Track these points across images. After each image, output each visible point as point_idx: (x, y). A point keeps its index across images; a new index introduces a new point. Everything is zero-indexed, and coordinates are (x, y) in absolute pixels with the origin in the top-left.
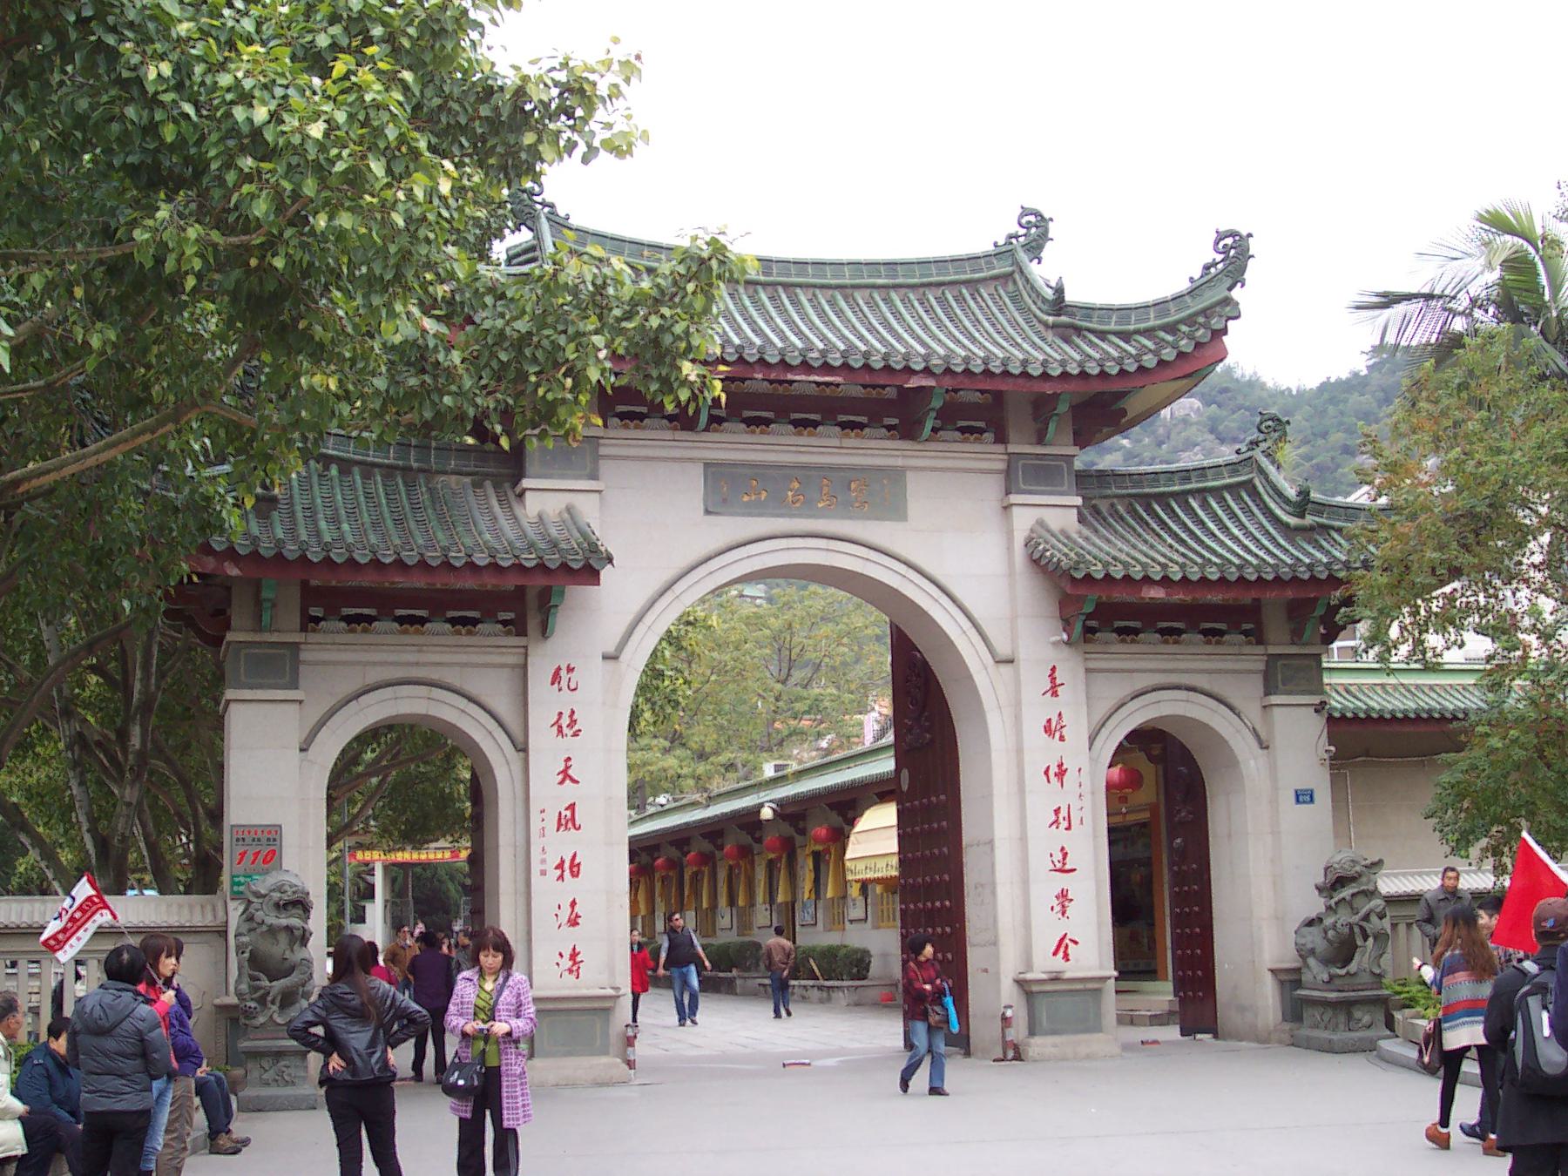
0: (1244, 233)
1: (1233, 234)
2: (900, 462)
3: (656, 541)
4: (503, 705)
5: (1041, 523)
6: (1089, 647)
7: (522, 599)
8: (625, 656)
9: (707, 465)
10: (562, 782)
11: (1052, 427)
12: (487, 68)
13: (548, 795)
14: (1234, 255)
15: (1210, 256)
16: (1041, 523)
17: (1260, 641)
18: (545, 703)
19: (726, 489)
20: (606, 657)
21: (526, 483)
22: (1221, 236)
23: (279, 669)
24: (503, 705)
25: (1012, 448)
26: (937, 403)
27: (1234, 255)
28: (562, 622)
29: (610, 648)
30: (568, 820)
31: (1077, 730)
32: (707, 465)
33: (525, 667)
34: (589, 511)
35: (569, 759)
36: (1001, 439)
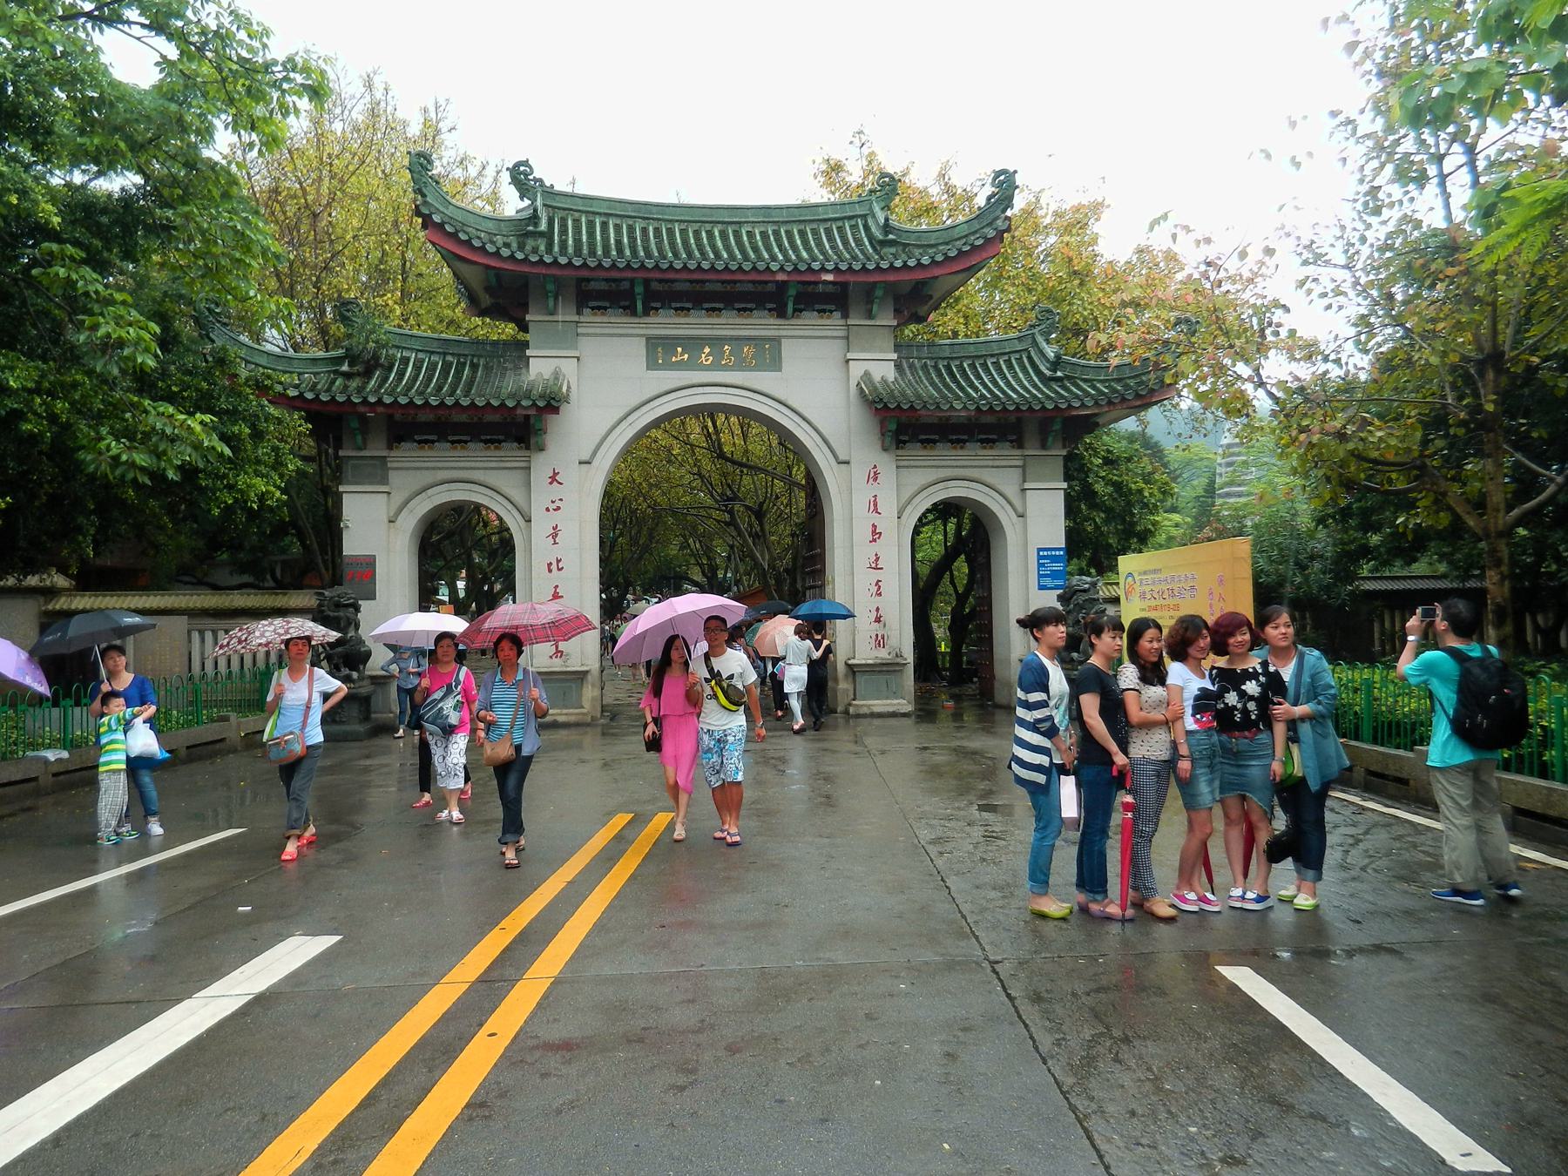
2: (776, 333)
3: (608, 389)
5: (867, 374)
6: (900, 452)
7: (520, 427)
8: (595, 463)
9: (649, 339)
11: (875, 308)
12: (916, 197)
16: (867, 374)
17: (1021, 446)
19: (659, 351)
21: (528, 353)
23: (377, 473)
24: (517, 496)
26: (792, 292)
28: (551, 440)
30: (876, 534)
31: (889, 506)
32: (649, 339)
34: (568, 368)
36: (845, 316)
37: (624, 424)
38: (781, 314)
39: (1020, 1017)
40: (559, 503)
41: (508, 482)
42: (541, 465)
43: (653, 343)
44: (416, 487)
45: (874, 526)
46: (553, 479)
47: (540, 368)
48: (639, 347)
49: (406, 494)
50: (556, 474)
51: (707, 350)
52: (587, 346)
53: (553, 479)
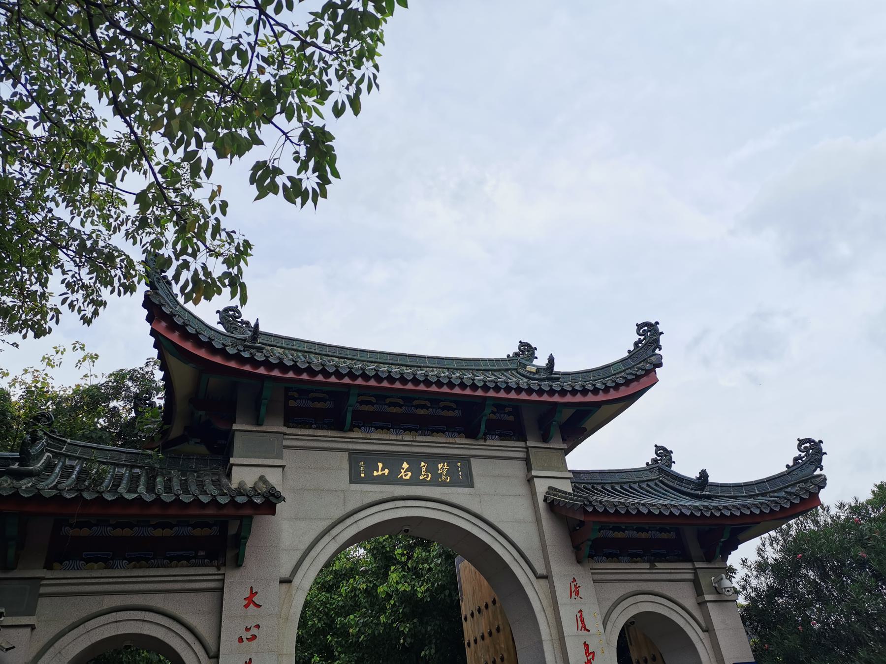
1: (809, 440)
8: (296, 581)
9: (352, 453)
10: (246, 606)
14: (650, 335)
15: (637, 338)
18: (234, 597)
19: (359, 467)
20: (282, 581)
22: (801, 442)
24: (203, 626)
25: (529, 444)
27: (650, 335)
29: (285, 572)
31: (594, 622)
32: (352, 453)
33: (221, 590)
37: (326, 539)
38: (472, 434)
39: (143, 621)
40: (254, 631)
41: (194, 611)
42: (236, 586)
43: (355, 457)
44: (615, 597)
45: (586, 645)
46: (250, 601)
47: (244, 476)
48: (342, 461)
49: (54, 630)
50: (253, 594)
51: (405, 465)
52: (289, 458)
53: (250, 601)
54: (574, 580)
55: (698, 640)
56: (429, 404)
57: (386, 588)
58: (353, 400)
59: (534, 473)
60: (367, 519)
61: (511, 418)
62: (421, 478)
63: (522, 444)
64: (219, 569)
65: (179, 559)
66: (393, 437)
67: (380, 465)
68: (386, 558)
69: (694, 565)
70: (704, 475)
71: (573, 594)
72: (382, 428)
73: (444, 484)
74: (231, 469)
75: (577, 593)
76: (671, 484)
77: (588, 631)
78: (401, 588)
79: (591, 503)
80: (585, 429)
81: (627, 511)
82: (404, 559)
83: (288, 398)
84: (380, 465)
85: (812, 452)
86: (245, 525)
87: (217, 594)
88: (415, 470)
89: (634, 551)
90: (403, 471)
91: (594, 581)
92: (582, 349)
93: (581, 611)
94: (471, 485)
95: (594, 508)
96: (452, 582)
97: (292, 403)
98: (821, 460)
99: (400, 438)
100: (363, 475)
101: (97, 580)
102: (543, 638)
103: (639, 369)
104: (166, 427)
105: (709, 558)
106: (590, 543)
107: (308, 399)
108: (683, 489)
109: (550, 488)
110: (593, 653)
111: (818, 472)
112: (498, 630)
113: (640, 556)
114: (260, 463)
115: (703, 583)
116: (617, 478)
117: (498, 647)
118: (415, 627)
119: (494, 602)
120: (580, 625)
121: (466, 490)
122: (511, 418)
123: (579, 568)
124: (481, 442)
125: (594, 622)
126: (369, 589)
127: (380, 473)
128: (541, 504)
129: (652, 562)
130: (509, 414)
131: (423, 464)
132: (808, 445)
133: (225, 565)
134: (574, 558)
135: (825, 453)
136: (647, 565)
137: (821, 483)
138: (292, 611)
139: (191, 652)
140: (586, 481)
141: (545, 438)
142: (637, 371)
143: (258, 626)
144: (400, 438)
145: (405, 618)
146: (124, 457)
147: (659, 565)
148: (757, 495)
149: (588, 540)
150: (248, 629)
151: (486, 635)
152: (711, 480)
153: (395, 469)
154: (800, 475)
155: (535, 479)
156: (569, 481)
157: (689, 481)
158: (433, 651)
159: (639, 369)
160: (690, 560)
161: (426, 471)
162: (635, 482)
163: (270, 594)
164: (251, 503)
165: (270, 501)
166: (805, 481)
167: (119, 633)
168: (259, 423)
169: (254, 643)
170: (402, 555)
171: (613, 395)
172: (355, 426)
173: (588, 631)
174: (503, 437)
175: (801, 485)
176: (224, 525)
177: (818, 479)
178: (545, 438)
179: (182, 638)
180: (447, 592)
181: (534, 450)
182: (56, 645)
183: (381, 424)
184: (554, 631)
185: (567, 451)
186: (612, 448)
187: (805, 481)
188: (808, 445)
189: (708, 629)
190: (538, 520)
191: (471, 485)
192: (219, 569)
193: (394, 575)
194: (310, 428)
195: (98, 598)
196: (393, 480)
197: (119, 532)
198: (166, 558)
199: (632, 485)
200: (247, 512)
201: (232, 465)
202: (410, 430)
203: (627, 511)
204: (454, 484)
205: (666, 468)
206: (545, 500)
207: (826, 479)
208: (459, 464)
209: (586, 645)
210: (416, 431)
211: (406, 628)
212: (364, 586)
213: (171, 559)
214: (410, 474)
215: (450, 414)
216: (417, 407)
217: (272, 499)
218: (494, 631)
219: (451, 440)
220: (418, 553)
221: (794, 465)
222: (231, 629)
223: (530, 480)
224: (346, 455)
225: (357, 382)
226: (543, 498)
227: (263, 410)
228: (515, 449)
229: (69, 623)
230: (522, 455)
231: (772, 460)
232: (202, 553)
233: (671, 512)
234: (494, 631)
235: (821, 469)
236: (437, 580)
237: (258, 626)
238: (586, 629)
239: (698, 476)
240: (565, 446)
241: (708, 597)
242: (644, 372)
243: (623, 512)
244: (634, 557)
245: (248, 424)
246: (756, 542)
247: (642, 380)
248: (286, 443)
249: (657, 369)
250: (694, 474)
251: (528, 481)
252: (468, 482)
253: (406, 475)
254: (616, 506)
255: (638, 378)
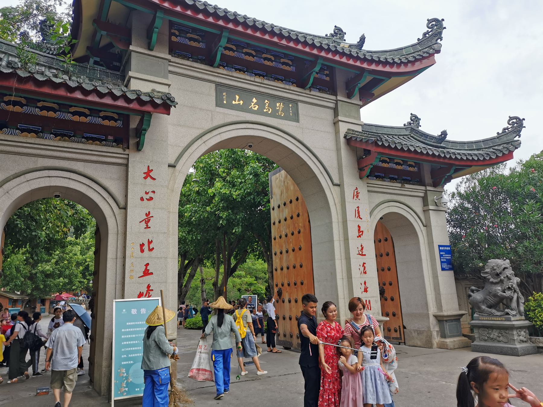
0: (440, 19)
1: (516, 118)
4: (115, 187)
8: (179, 167)
10: (145, 178)
13: (136, 233)
14: (436, 27)
18: (137, 187)
20: (169, 166)
22: (511, 118)
24: (115, 187)
25: (339, 98)
27: (436, 27)
33: (127, 165)
35: (147, 265)
37: (199, 142)
38: (302, 84)
39: (69, 179)
42: (138, 163)
44: (377, 201)
45: (359, 227)
46: (148, 174)
50: (150, 171)
51: (254, 100)
53: (148, 174)
54: (357, 189)
55: (420, 230)
56: (273, 59)
57: (214, 191)
58: (223, 42)
59: (340, 118)
60: (227, 133)
61: (328, 79)
62: (265, 111)
63: (333, 97)
64: (124, 151)
65: (94, 139)
66: (248, 77)
67: (237, 97)
68: (211, 174)
69: (426, 188)
70: (444, 134)
71: (355, 197)
72: (240, 70)
73: (279, 117)
74: (129, 81)
75: (357, 197)
76: (419, 139)
77: (361, 219)
78: (223, 191)
79: (381, 139)
80: (373, 95)
81: (402, 148)
82: (224, 175)
83: (171, 34)
84: (237, 97)
85: (517, 125)
86: (145, 119)
87: (123, 168)
88: (261, 104)
89: (392, 176)
90: (253, 104)
91: (368, 191)
92: (385, 34)
93: (358, 207)
94: (297, 121)
95: (383, 143)
96: (263, 190)
97: (174, 39)
98: (520, 131)
99: (252, 79)
100: (225, 102)
101: (31, 145)
102: (333, 220)
103: (424, 53)
104: (74, 41)
105: (435, 185)
106: (372, 166)
107: (186, 38)
108: (426, 142)
109: (349, 130)
110: (362, 231)
111: (517, 138)
112: (298, 216)
113: (396, 179)
114: (152, 79)
115: (430, 199)
116: (385, 131)
117: (296, 225)
118: (229, 215)
119: (297, 199)
120: (357, 215)
121: (294, 124)
122: (328, 79)
123: (360, 181)
124: (307, 92)
125: (365, 213)
126: (200, 191)
127: (237, 103)
128: (342, 140)
129: (403, 184)
130: (327, 75)
131: (266, 101)
132: (515, 121)
133: (128, 148)
134: (358, 175)
135: (525, 127)
136: (400, 185)
137: (517, 145)
138: (176, 186)
139: (106, 203)
140: (367, 130)
141: (349, 95)
142: (419, 57)
143: (154, 192)
144: (252, 79)
145: (224, 209)
146: (42, 59)
147: (407, 186)
148: (474, 150)
149: (372, 164)
150: (147, 193)
151: (289, 218)
152: (448, 138)
153: (248, 102)
154: (505, 139)
155: (340, 123)
156: (361, 127)
157: (432, 137)
158: (240, 230)
159: (424, 53)
160: (423, 184)
161: (268, 106)
162: (396, 135)
163: (161, 172)
164: (152, 103)
165: (166, 105)
166: (508, 143)
167: (52, 185)
168: (150, 48)
169: (152, 201)
170: (224, 172)
171: (402, 69)
172: (220, 65)
173: (361, 219)
174: (320, 90)
175: (505, 145)
176: (126, 120)
177: (516, 143)
178: (349, 95)
179: (99, 193)
180: (252, 197)
181: (341, 103)
182: (4, 187)
183: (239, 67)
184: (340, 217)
185: (361, 107)
186: (384, 112)
187: (508, 143)
188: (515, 121)
189: (427, 225)
190: (338, 150)
191: (297, 121)
192: (124, 151)
193: (219, 184)
194: (188, 60)
195: (33, 158)
196: (245, 109)
197: (44, 113)
198: (83, 137)
199: (394, 136)
200: (148, 108)
201: (130, 77)
202: (260, 75)
203: (402, 148)
204: (286, 118)
205: (416, 129)
206: (345, 137)
207: (521, 143)
208: (290, 105)
209: (359, 227)
210: (264, 76)
211: (224, 215)
212: (197, 189)
213: (88, 139)
214: (257, 107)
215: (287, 68)
216: (265, 59)
217: (168, 102)
218: (295, 216)
219: (287, 87)
220: (234, 172)
221: (503, 132)
222: (136, 190)
223: (336, 123)
224: (213, 86)
225: (131, 106)
226: (343, 136)
227: (155, 37)
228: (328, 99)
229: (12, 173)
230: (332, 105)
231: (488, 128)
232: (110, 138)
233: (427, 152)
234: (295, 216)
235: (520, 137)
236: (247, 188)
237: (154, 192)
238: (360, 218)
239: (440, 134)
240: (361, 103)
241: (431, 207)
242: (428, 55)
243: (399, 148)
244: (392, 179)
245: (141, 47)
246: (459, 179)
247: (424, 61)
248: (171, 68)
249: (435, 55)
250: (436, 133)
251: (334, 123)
252: (296, 118)
253: (254, 107)
254: (396, 143)
255: (424, 58)
